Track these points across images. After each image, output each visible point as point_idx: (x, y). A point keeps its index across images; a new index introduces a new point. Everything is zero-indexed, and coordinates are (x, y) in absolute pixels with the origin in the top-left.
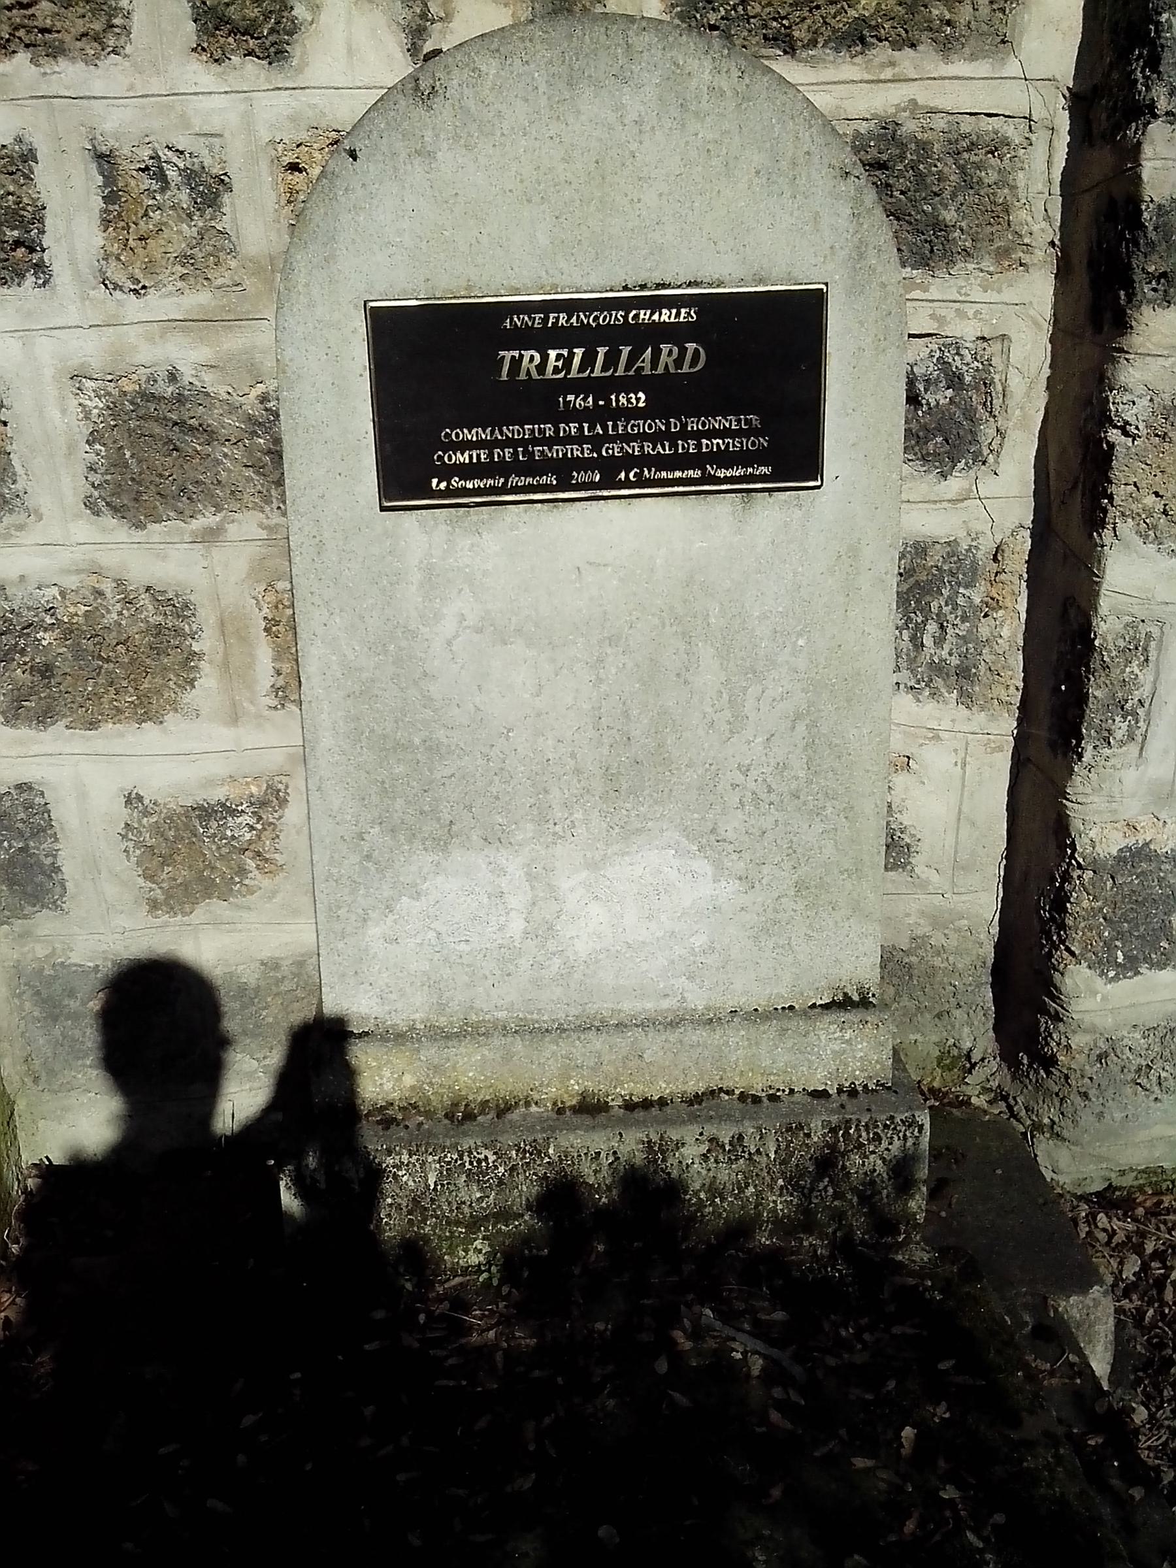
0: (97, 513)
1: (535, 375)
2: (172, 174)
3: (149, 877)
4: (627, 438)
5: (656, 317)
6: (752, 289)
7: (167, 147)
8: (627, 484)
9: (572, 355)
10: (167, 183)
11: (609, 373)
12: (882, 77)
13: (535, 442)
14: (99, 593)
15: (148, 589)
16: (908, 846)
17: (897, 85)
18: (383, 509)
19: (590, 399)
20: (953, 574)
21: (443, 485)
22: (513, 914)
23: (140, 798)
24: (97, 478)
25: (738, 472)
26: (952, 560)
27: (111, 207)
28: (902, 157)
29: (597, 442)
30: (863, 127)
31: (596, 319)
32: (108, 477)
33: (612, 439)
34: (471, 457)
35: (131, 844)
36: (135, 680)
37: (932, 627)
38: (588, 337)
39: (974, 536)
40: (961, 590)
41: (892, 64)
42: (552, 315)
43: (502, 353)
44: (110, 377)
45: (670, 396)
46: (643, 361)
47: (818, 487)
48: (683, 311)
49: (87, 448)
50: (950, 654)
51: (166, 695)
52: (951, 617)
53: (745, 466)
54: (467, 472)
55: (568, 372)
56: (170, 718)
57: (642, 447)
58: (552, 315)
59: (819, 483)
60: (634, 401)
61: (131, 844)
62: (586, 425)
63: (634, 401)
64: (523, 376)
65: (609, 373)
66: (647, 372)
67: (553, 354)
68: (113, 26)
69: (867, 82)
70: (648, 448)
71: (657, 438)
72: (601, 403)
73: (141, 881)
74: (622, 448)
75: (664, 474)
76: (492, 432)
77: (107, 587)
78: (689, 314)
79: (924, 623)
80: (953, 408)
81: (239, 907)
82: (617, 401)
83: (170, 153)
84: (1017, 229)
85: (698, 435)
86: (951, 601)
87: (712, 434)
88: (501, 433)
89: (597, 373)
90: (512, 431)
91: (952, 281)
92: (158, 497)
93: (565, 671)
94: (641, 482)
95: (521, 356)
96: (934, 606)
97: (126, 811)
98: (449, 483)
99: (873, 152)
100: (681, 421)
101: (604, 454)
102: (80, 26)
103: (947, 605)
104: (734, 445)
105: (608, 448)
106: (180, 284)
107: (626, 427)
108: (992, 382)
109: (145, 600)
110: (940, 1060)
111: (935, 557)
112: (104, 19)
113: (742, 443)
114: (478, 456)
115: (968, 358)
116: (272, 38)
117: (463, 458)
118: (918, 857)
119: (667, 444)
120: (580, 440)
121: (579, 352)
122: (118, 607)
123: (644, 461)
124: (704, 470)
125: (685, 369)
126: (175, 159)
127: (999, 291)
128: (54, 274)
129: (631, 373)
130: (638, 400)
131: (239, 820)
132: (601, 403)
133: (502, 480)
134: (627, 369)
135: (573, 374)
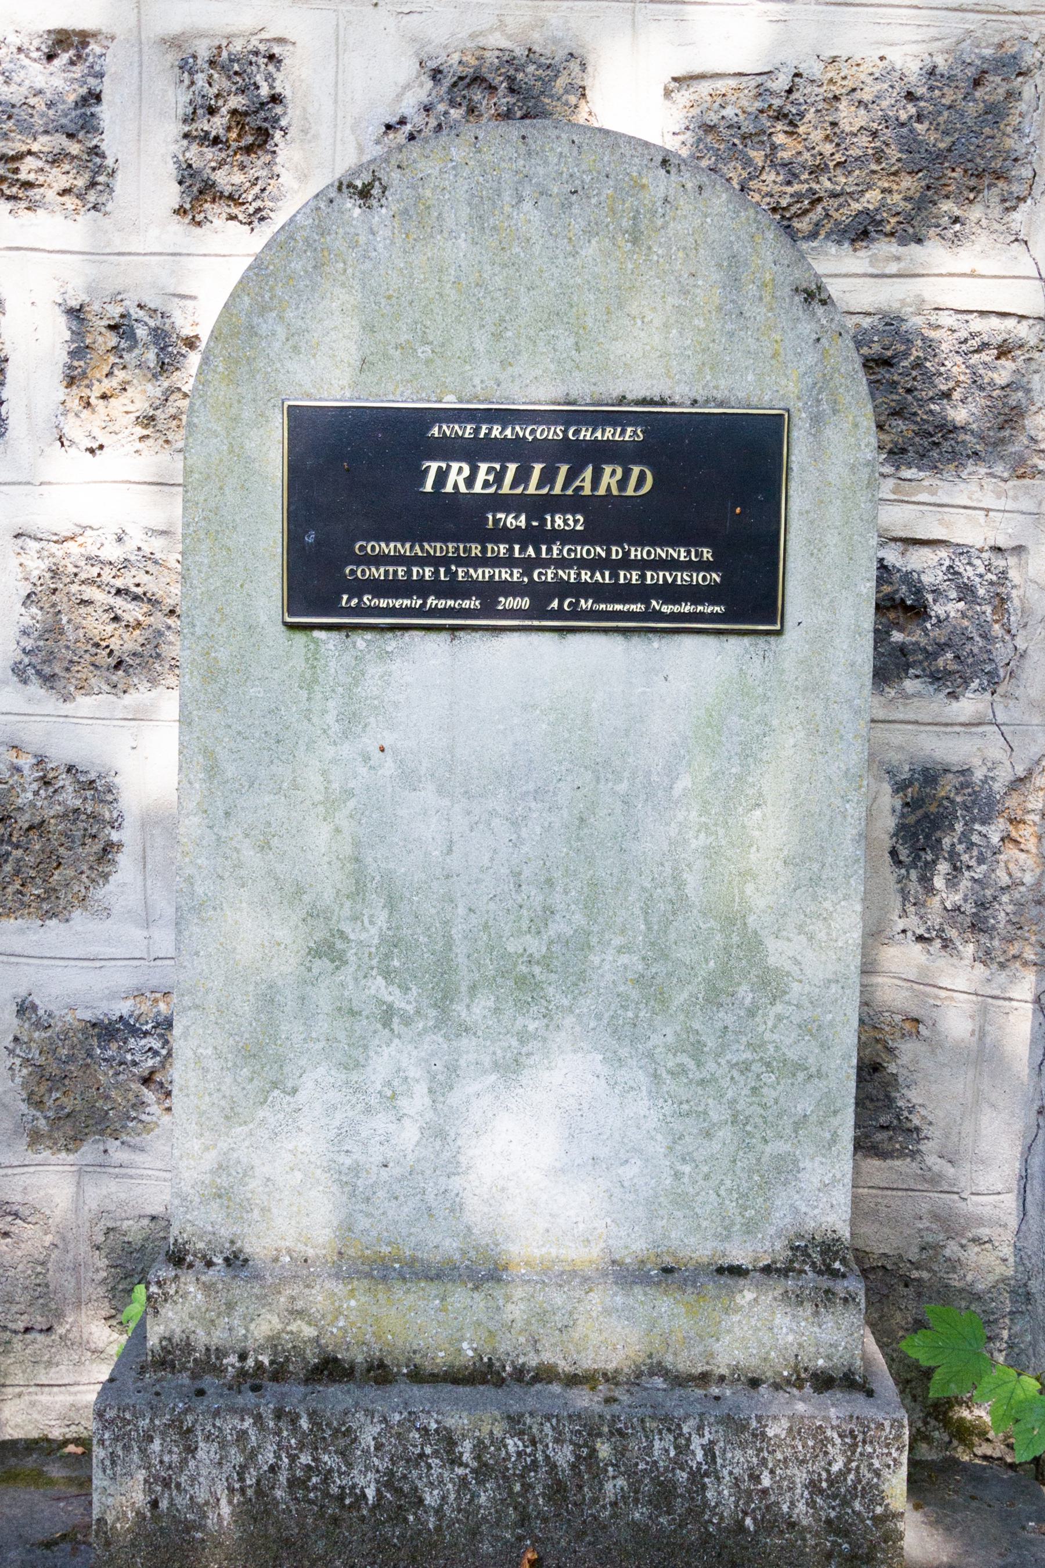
0: (25, 682)
1: (463, 489)
2: (141, 332)
3: (35, 1101)
4: (562, 563)
5: (598, 434)
6: (706, 411)
7: (139, 306)
8: (560, 614)
9: (504, 469)
10: (136, 341)
11: (545, 491)
12: (887, 271)
13: (459, 561)
14: (18, 770)
15: (70, 769)
16: (917, 1129)
17: (902, 280)
18: (291, 627)
19: (523, 518)
20: (967, 809)
21: (354, 602)
22: (406, 1121)
23: (34, 1007)
24: (28, 643)
25: (687, 608)
26: (966, 791)
27: (76, 364)
28: (906, 354)
29: (528, 565)
30: (866, 322)
31: (533, 432)
32: (41, 643)
33: (546, 563)
34: (386, 572)
35: (18, 1061)
36: (45, 870)
37: (943, 867)
38: (519, 452)
39: (989, 764)
40: (977, 826)
41: (898, 259)
42: (484, 427)
43: (427, 464)
44: (55, 538)
45: (608, 520)
46: (583, 480)
47: (779, 633)
48: (629, 429)
49: (23, 610)
50: (965, 900)
51: (76, 889)
52: (965, 857)
53: (695, 603)
54: (381, 589)
55: (499, 487)
56: (77, 914)
57: (579, 575)
58: (484, 427)
59: (778, 627)
60: (571, 522)
61: (18, 1061)
62: (517, 547)
63: (571, 522)
64: (449, 488)
65: (545, 491)
66: (587, 491)
67: (483, 467)
68: (97, 184)
69: (872, 276)
70: (585, 576)
71: (595, 565)
72: (535, 524)
73: (24, 1107)
74: (556, 574)
75: (603, 607)
76: (412, 548)
77: (26, 762)
78: (635, 432)
79: (934, 862)
80: (966, 623)
81: (133, 1148)
82: (553, 521)
83: (141, 313)
84: (1033, 433)
85: (643, 565)
86: (965, 837)
87: (659, 565)
88: (422, 548)
89: (532, 490)
90: (435, 549)
91: (963, 486)
92: (92, 668)
93: (481, 826)
94: (576, 614)
95: (449, 467)
96: (947, 842)
97: (16, 1021)
98: (361, 600)
99: (876, 348)
100: (623, 548)
101: (536, 578)
102: (64, 182)
103: (960, 843)
104: (682, 578)
105: (540, 574)
106: (139, 446)
107: (561, 551)
108: (1009, 598)
109: (64, 780)
110: (795, 1162)
111: (947, 786)
112: (87, 176)
113: (691, 577)
114: (395, 572)
115: (981, 570)
116: (258, 204)
117: (378, 573)
118: (930, 1144)
119: (607, 573)
120: (510, 562)
121: (512, 468)
122: (35, 786)
123: (581, 590)
124: (648, 604)
125: (630, 492)
126: (146, 319)
127: (1015, 498)
128: (10, 427)
129: (570, 492)
130: (576, 521)
131: (143, 1042)
132: (535, 524)
133: (420, 602)
134: (565, 487)
135: (506, 489)
